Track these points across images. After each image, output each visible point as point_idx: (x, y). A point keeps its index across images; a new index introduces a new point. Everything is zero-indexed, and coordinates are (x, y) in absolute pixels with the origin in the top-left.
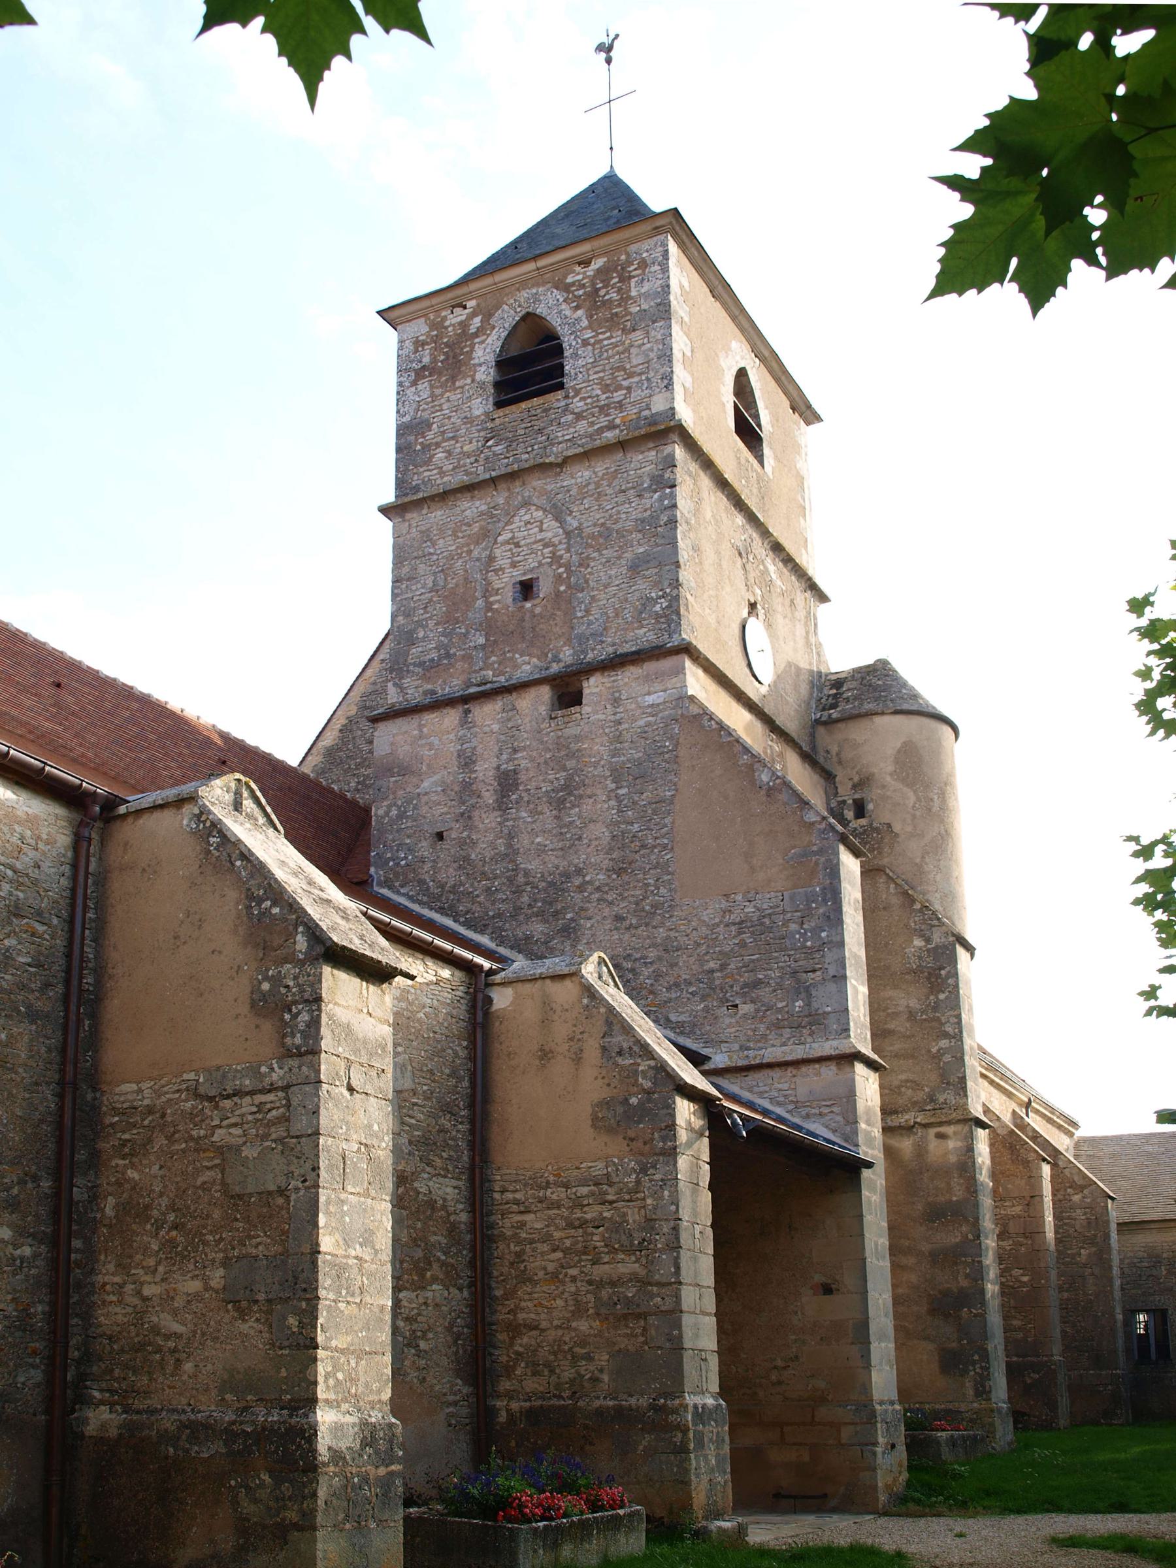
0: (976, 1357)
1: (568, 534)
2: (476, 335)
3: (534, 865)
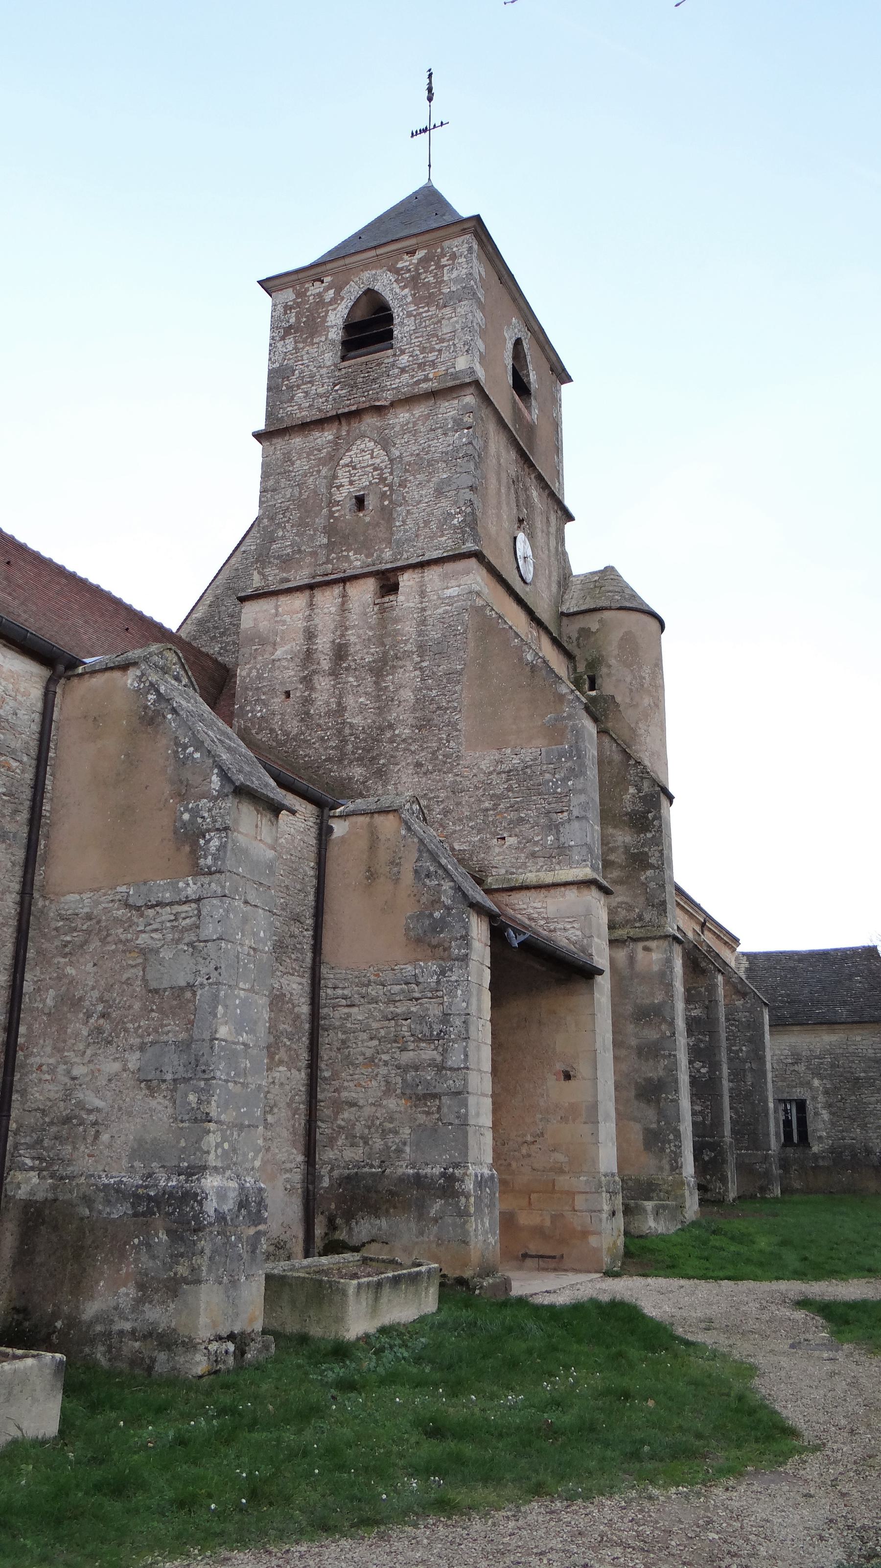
0: (671, 1137)
1: (391, 461)
2: (330, 303)
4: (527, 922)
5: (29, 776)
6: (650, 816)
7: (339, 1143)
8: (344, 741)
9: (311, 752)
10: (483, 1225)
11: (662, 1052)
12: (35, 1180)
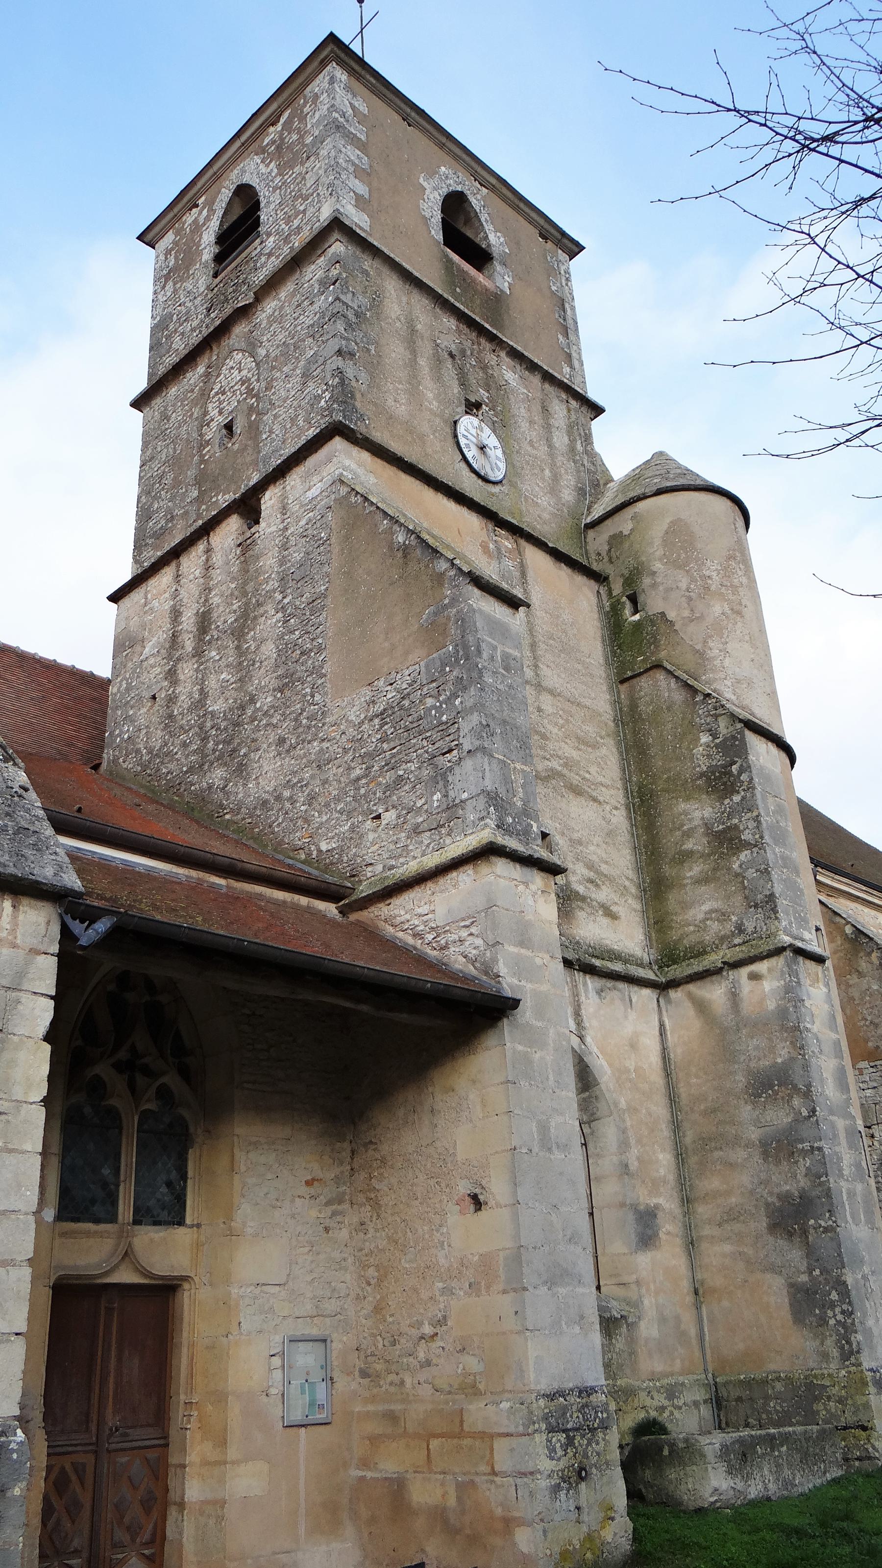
4: (410, 940)
11: (800, 1146)
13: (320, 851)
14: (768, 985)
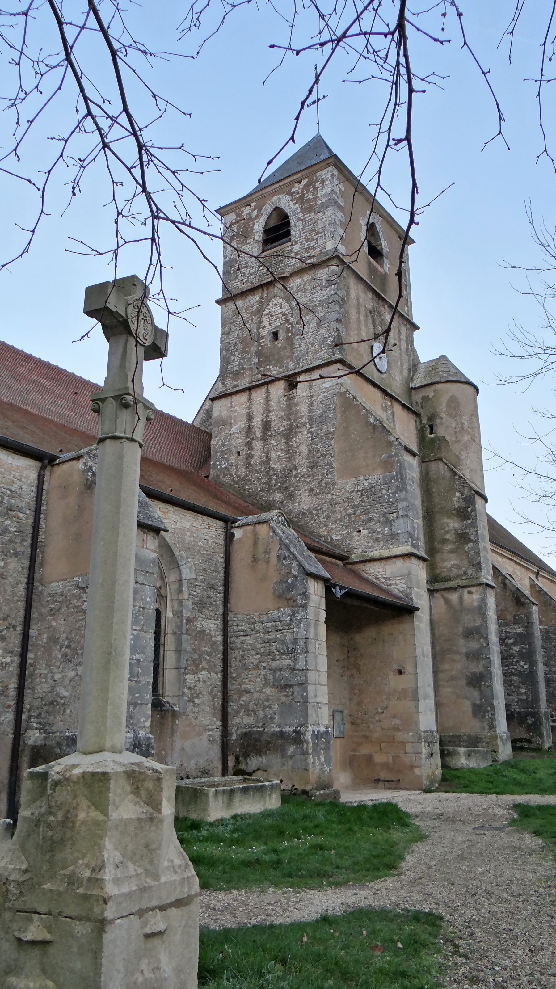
2: (255, 219)
3: (277, 466)
4: (375, 580)
5: (30, 521)
6: (469, 509)
7: (241, 714)
8: (270, 479)
9: (252, 486)
10: (319, 759)
12: (37, 735)
13: (332, 539)
14: (475, 596)
